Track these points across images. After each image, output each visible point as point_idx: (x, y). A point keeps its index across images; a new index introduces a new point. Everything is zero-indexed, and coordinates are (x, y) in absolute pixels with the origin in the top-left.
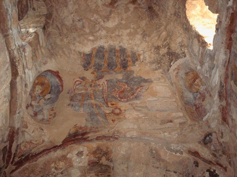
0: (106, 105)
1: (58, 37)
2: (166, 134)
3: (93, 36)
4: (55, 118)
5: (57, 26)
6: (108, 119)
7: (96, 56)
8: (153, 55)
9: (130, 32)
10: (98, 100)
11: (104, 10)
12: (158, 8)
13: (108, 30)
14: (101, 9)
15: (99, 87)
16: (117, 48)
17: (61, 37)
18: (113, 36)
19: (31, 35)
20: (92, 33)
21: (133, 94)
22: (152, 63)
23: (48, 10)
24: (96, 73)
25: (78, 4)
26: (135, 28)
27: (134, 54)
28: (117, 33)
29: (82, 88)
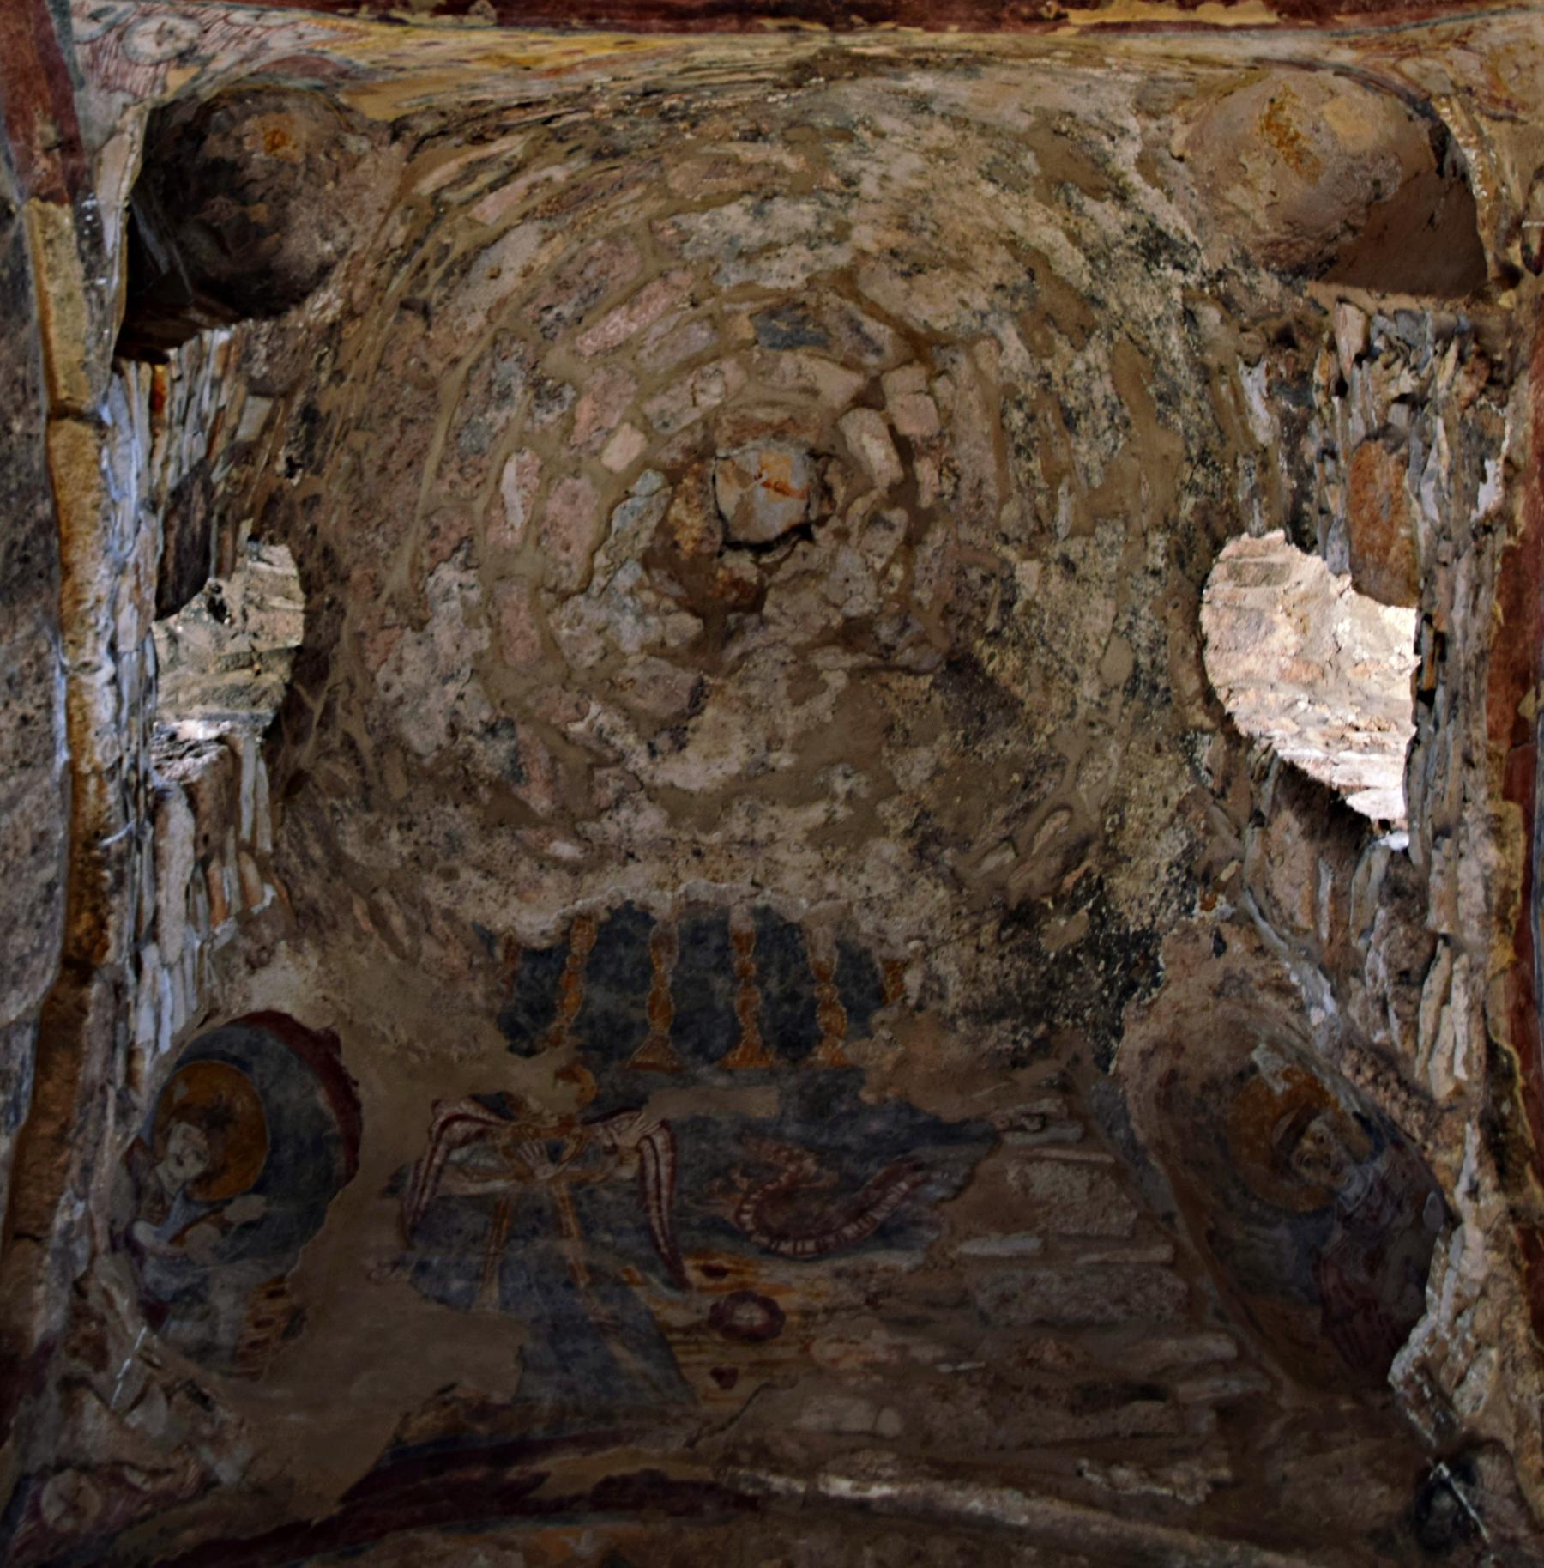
0: (664, 1272)
1: (350, 813)
2: (1121, 1474)
3: (578, 837)
4: (292, 1342)
5: (350, 744)
6: (686, 1365)
7: (594, 969)
8: (989, 965)
9: (826, 825)
10: (608, 1238)
11: (654, 679)
12: (1013, 661)
13: (676, 803)
14: (637, 673)
15: (612, 1161)
16: (741, 921)
17: (371, 818)
18: (711, 848)
19: (195, 748)
20: (567, 821)
21: (861, 1212)
22: (983, 1015)
23: (311, 617)
24: (589, 1075)
25: (490, 625)
26: (864, 793)
27: (855, 959)
28: (738, 827)
29: (491, 1163)
